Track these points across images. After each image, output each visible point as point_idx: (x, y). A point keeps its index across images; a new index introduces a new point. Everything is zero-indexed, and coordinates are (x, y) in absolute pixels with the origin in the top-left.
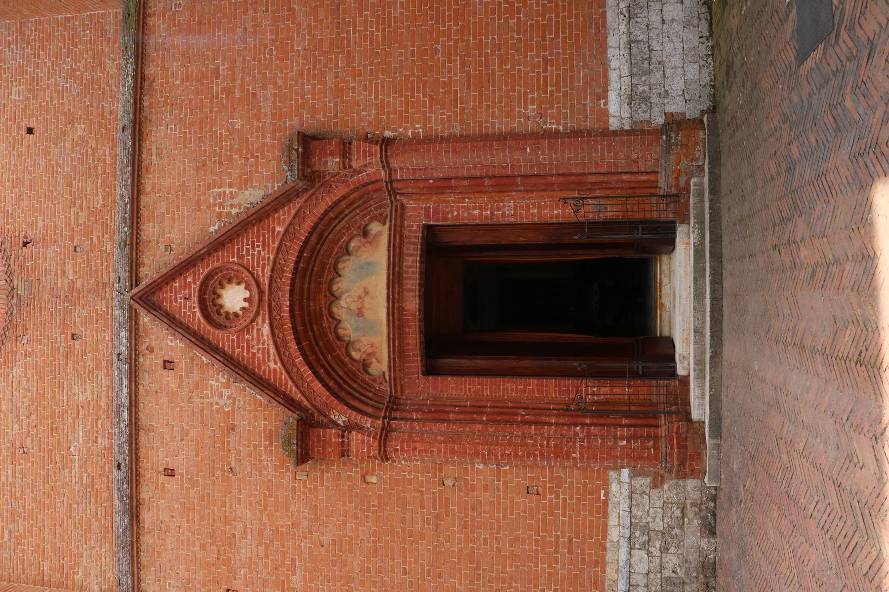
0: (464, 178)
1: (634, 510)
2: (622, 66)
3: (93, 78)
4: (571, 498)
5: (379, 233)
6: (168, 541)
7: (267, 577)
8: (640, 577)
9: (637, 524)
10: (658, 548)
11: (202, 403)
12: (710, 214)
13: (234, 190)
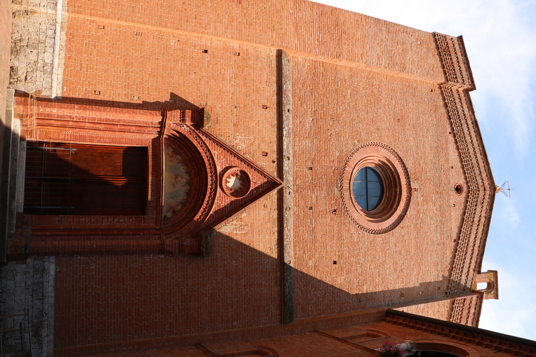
0: (126, 235)
1: (50, 80)
2: (47, 287)
3: (307, 287)
4: (80, 88)
5: (167, 212)
6: (266, 77)
7: (221, 60)
8: (48, 51)
9: (49, 74)
10: (39, 63)
11: (249, 137)
12: (6, 214)
13: (235, 232)
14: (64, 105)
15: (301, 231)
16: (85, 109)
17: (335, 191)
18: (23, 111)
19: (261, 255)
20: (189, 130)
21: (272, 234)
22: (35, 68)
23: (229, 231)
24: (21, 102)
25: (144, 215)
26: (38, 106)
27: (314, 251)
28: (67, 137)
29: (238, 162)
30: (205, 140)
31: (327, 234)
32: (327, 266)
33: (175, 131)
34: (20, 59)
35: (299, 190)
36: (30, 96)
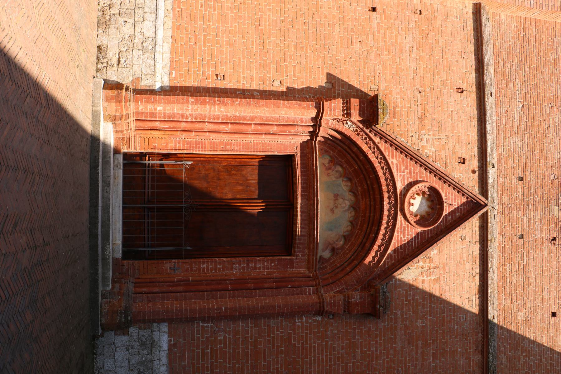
2: (159, 367)
3: (515, 352)
5: (324, 250)
10: (136, 38)
11: (439, 135)
12: (98, 265)
13: (421, 278)
14: (173, 98)
15: (508, 271)
16: (204, 103)
17: (555, 210)
18: (116, 111)
19: (456, 309)
20: (355, 129)
21: (471, 279)
22: (131, 46)
23: (413, 276)
24: (112, 98)
25: (290, 254)
26: (137, 101)
27: (525, 299)
28: (178, 145)
29: (426, 175)
30: (379, 143)
31: (544, 274)
32: (543, 320)
33: (335, 131)
34: (109, 33)
35: (506, 211)
36: (125, 88)
